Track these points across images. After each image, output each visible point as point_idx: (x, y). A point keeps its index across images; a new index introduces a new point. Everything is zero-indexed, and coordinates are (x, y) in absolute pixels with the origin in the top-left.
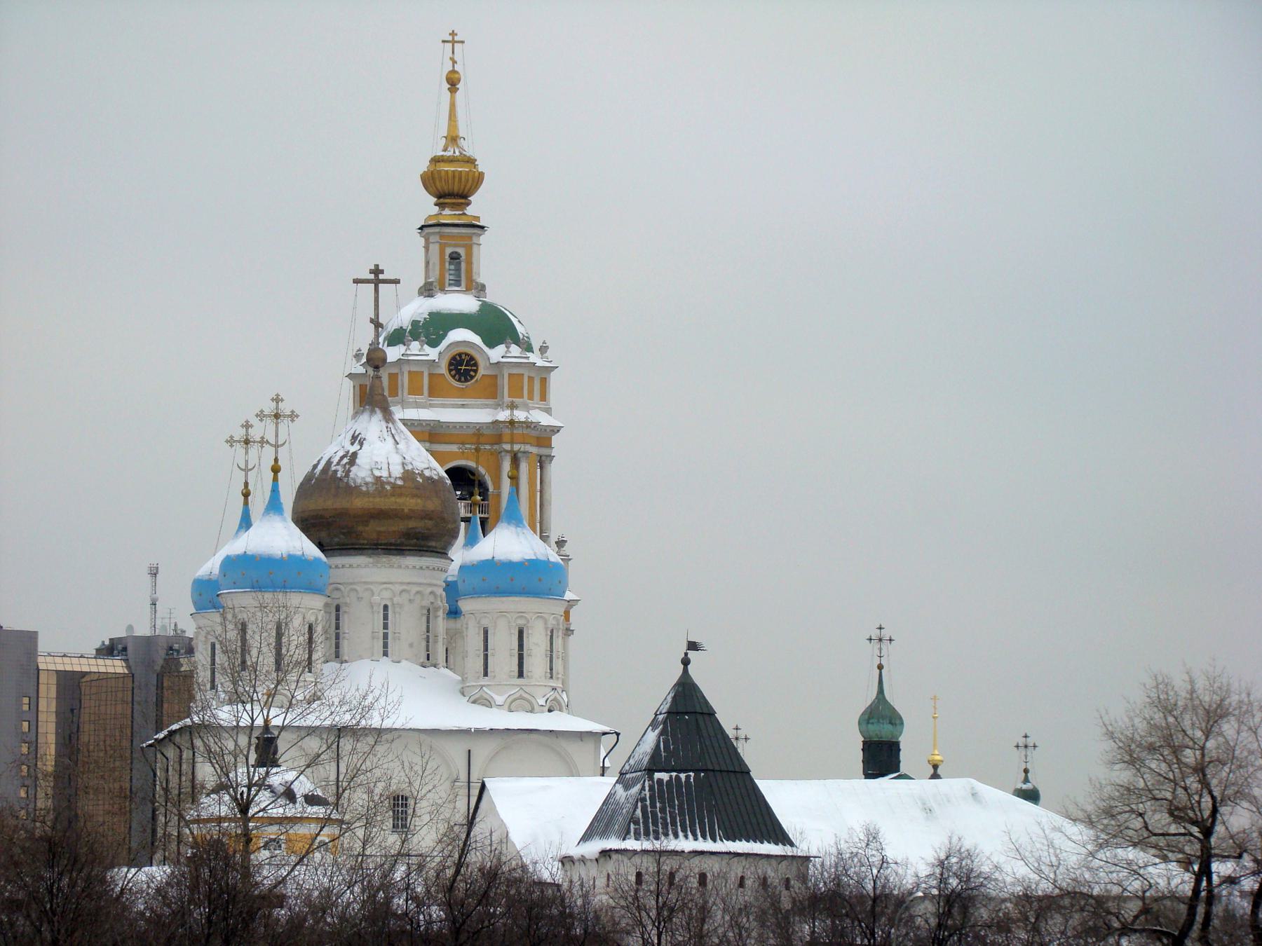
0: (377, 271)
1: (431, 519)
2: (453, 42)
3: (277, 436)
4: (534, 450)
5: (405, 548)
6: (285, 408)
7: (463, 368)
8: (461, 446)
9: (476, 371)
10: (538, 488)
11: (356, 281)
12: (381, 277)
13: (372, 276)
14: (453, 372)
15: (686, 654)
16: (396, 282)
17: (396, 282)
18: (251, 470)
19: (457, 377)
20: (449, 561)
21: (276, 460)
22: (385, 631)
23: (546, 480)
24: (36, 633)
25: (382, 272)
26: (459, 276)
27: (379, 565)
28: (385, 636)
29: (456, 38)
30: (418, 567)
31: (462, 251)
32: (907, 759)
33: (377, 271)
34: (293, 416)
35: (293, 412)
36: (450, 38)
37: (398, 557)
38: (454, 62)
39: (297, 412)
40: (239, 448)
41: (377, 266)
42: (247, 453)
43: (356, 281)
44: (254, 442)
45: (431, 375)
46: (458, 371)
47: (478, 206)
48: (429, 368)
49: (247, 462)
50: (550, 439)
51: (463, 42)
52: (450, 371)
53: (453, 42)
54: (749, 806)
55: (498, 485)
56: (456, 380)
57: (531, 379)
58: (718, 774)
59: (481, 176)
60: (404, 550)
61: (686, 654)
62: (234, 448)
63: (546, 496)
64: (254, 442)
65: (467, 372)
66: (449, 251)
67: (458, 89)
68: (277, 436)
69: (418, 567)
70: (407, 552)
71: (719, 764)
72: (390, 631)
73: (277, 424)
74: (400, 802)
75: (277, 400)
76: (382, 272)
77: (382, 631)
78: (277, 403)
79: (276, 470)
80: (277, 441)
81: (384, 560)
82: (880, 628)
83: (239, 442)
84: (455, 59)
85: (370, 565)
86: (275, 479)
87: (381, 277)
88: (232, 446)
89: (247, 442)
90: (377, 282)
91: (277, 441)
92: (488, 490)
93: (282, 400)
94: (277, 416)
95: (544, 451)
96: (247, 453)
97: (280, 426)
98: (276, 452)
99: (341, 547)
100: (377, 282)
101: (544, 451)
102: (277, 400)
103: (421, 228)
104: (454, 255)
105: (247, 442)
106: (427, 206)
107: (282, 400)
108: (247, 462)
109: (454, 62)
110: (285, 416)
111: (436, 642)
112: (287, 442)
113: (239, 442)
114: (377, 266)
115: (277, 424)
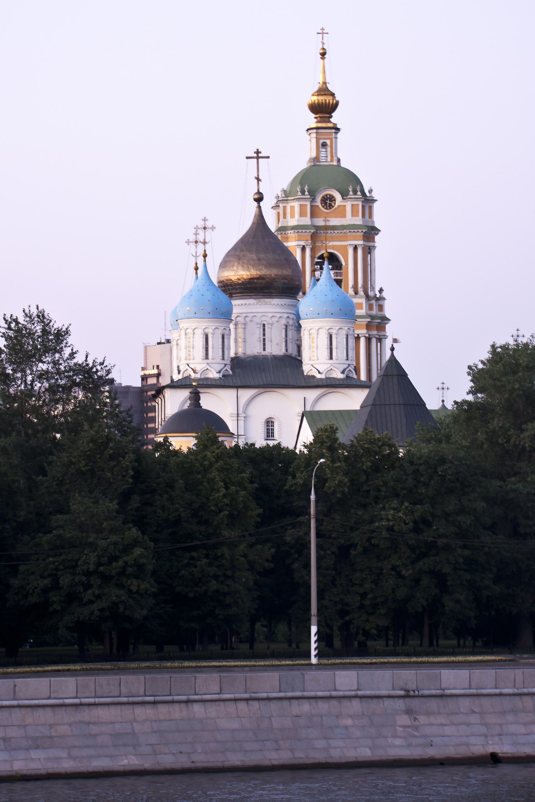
0: (258, 152)
1: (286, 279)
5: (273, 295)
6: (209, 224)
7: (328, 202)
8: (306, 242)
10: (369, 263)
11: (248, 158)
13: (255, 155)
14: (323, 205)
15: (392, 345)
16: (268, 157)
17: (268, 157)
18: (198, 256)
20: (297, 301)
22: (264, 337)
23: (372, 259)
24: (468, 366)
25: (260, 153)
26: (326, 154)
28: (264, 340)
29: (324, 32)
30: (244, 304)
31: (328, 142)
32: (148, 368)
33: (258, 152)
34: (213, 228)
36: (321, 32)
39: (215, 226)
40: (193, 245)
43: (248, 158)
45: (312, 207)
47: (336, 118)
50: (374, 238)
52: (321, 204)
55: (347, 264)
56: (325, 208)
59: (337, 104)
60: (273, 295)
61: (392, 345)
62: (190, 245)
63: (373, 267)
65: (326, 203)
66: (321, 141)
67: (325, 57)
69: (244, 304)
70: (274, 297)
72: (266, 337)
73: (205, 232)
74: (270, 424)
75: (205, 220)
76: (260, 153)
77: (262, 337)
79: (205, 256)
82: (518, 330)
83: (192, 242)
84: (324, 42)
88: (188, 244)
90: (258, 158)
92: (342, 265)
93: (207, 220)
95: (370, 244)
99: (264, 294)
100: (258, 158)
101: (370, 244)
102: (205, 220)
103: (308, 130)
104: (324, 144)
105: (196, 242)
106: (311, 120)
110: (209, 228)
111: (229, 339)
112: (210, 242)
113: (192, 242)
115: (205, 232)
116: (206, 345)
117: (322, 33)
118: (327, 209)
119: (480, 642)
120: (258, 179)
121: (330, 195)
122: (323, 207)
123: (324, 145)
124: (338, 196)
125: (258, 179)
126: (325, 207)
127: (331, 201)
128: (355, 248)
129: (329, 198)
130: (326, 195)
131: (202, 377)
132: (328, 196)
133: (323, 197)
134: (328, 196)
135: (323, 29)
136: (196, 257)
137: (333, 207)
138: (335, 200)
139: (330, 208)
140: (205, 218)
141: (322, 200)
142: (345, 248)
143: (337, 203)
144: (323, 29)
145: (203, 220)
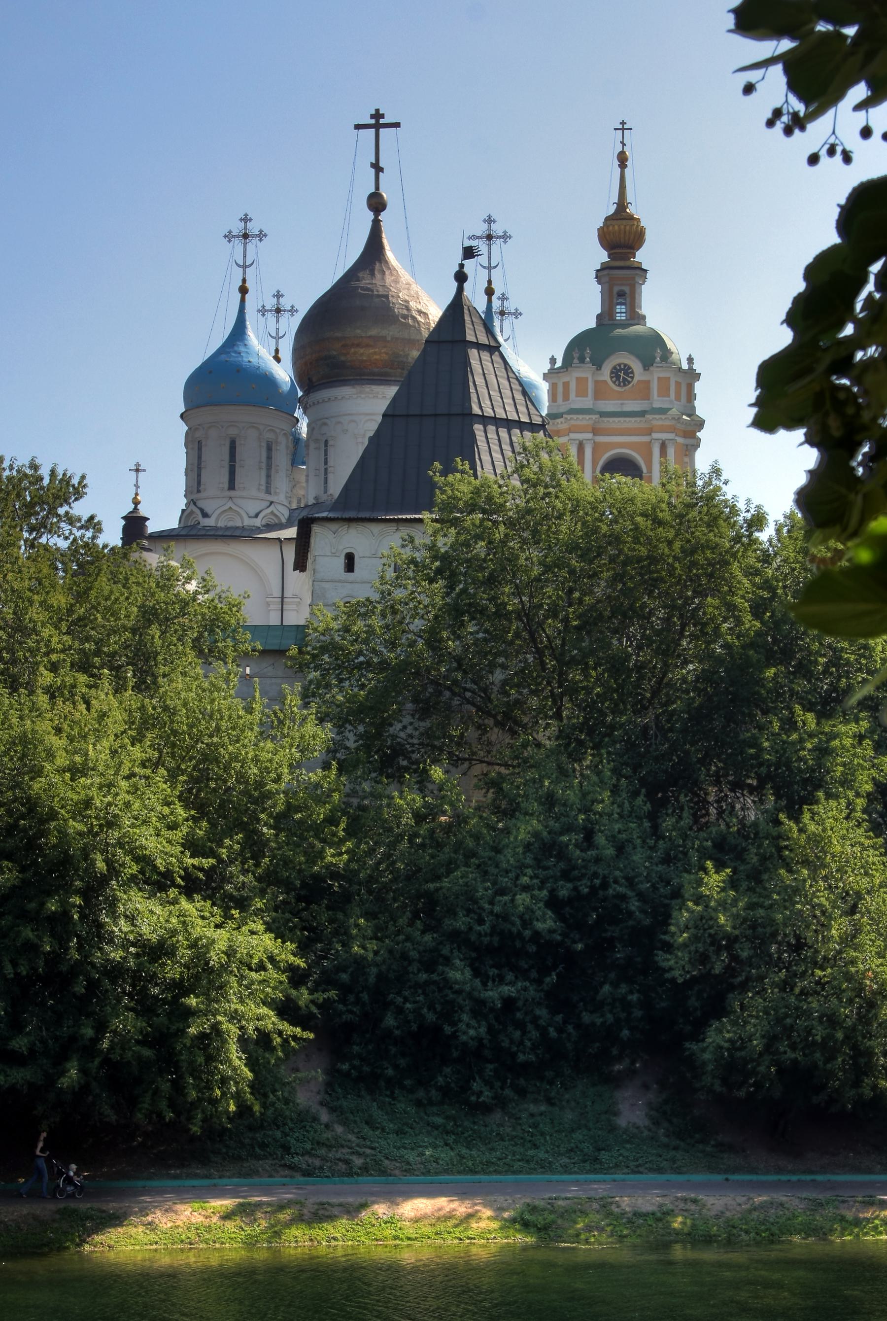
0: (377, 115)
2: (623, 129)
3: (245, 256)
4: (680, 440)
6: (254, 228)
9: (632, 378)
11: (358, 127)
12: (382, 121)
13: (373, 121)
14: (614, 379)
15: (462, 266)
16: (397, 125)
17: (397, 125)
18: (281, 337)
19: (617, 383)
21: (244, 281)
25: (382, 116)
27: (363, 396)
29: (625, 126)
31: (626, 289)
33: (377, 115)
35: (261, 231)
36: (621, 126)
37: (382, 387)
38: (624, 144)
39: (265, 231)
41: (377, 110)
42: (278, 321)
43: (358, 127)
44: (285, 311)
45: (596, 383)
46: (618, 377)
48: (593, 374)
49: (277, 329)
51: (631, 129)
52: (611, 378)
53: (623, 129)
54: (495, 447)
55: (650, 471)
57: (678, 384)
58: (491, 428)
61: (462, 266)
64: (285, 311)
65: (618, 377)
66: (616, 289)
68: (245, 256)
71: (481, 408)
73: (245, 244)
76: (382, 116)
78: (246, 223)
80: (245, 262)
81: (368, 390)
83: (271, 311)
85: (355, 396)
86: (243, 300)
87: (382, 121)
89: (278, 311)
90: (377, 127)
91: (245, 262)
94: (246, 236)
96: (278, 321)
97: (249, 246)
98: (244, 273)
102: (246, 219)
105: (278, 311)
107: (251, 220)
108: (277, 329)
109: (624, 144)
113: (271, 311)
114: (377, 110)
115: (245, 244)
116: (230, 461)
117: (623, 128)
118: (619, 385)
119: (347, 1064)
120: (377, 168)
121: (625, 365)
122: (614, 383)
123: (621, 294)
124: (636, 366)
125: (377, 168)
126: (617, 383)
127: (626, 373)
128: (663, 447)
129: (623, 369)
130: (619, 365)
131: (219, 525)
132: (622, 366)
133: (615, 368)
134: (622, 366)
135: (623, 123)
136: (277, 338)
137: (629, 382)
138: (632, 372)
139: (625, 385)
140: (246, 215)
141: (612, 372)
142: (648, 446)
143: (637, 378)
144: (623, 123)
145: (241, 220)
